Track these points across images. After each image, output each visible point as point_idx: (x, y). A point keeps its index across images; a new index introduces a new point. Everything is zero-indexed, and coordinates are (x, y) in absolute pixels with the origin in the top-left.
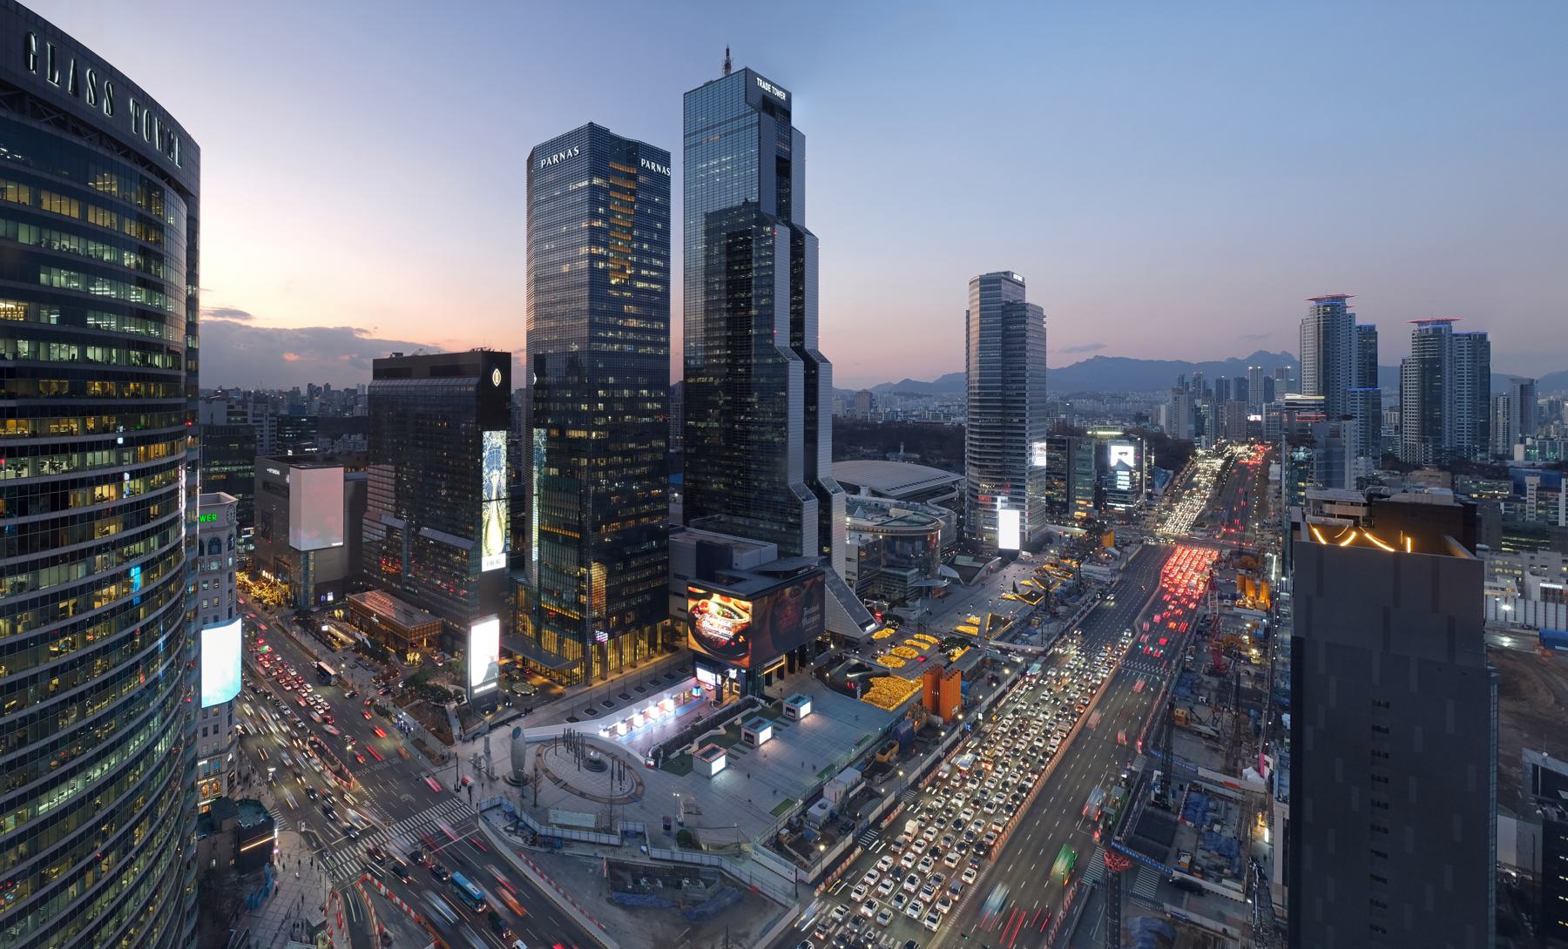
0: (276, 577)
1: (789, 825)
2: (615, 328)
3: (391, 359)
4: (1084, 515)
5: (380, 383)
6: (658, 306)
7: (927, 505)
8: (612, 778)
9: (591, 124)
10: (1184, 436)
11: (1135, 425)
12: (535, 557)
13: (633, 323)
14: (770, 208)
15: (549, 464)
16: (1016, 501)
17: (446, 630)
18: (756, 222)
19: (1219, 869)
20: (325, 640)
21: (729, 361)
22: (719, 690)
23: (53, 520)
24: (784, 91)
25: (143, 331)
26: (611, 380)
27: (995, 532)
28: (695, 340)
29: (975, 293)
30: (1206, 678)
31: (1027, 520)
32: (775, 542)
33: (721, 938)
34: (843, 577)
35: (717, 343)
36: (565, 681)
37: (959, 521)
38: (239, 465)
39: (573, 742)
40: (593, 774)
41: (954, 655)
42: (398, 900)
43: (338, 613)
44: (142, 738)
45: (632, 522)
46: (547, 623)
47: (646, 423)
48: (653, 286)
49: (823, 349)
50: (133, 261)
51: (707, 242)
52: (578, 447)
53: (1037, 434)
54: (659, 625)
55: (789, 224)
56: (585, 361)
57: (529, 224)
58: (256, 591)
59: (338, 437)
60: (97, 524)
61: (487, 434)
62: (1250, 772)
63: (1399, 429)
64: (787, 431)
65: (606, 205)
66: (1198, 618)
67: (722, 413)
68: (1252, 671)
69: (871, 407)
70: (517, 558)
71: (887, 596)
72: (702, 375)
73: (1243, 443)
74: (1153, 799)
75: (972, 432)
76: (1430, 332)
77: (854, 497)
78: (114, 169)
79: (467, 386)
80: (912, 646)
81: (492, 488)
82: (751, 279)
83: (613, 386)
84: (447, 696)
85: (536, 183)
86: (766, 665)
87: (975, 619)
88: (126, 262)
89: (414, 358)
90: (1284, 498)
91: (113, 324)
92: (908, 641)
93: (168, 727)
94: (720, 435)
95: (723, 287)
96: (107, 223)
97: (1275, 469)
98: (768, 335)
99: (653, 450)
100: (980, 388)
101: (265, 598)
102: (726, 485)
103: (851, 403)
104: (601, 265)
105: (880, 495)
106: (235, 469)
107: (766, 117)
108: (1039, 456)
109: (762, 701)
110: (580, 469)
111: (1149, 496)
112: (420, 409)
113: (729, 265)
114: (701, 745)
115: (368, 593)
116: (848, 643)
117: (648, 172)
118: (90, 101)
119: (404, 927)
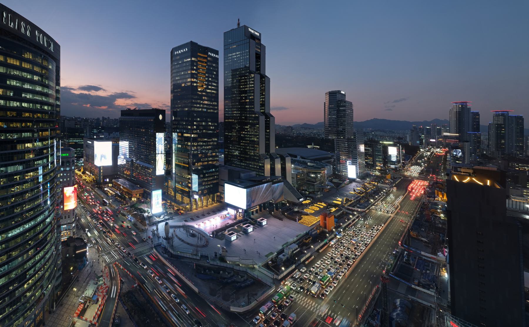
0: (91, 173)
1: (272, 260)
2: (200, 104)
3: (127, 110)
4: (380, 168)
6: (215, 98)
7: (322, 162)
8: (198, 239)
9: (191, 41)
11: (397, 141)
12: (174, 172)
13: (206, 102)
14: (253, 68)
15: (178, 144)
16: (353, 163)
17: (145, 192)
19: (429, 285)
20: (106, 193)
22: (236, 216)
23: (12, 153)
25: (41, 99)
26: (198, 119)
27: (347, 172)
29: (327, 97)
30: (424, 223)
31: (358, 169)
32: (256, 171)
33: (247, 295)
36: (184, 209)
37: (333, 168)
39: (187, 228)
41: (332, 210)
42: (126, 271)
43: (110, 185)
44: (42, 217)
45: (206, 163)
46: (178, 192)
47: (210, 133)
48: (213, 91)
50: (37, 78)
51: (232, 78)
52: (188, 139)
54: (216, 195)
58: (84, 177)
60: (26, 154)
61: (157, 134)
62: (440, 254)
65: (196, 66)
66: (421, 203)
70: (168, 172)
71: (308, 190)
73: (438, 148)
74: (405, 261)
76: (500, 115)
77: (295, 159)
78: (31, 52)
80: (317, 206)
83: (199, 121)
84: (145, 212)
85: (173, 59)
86: (251, 209)
88: (35, 79)
89: (135, 110)
91: (31, 96)
92: (315, 205)
93: (51, 214)
96: (28, 67)
97: (448, 156)
99: (212, 141)
101: (87, 179)
102: (239, 153)
103: (284, 130)
104: (195, 84)
105: (304, 159)
106: (77, 141)
107: (251, 40)
108: (362, 148)
109: (250, 220)
110: (188, 146)
111: (403, 163)
114: (229, 231)
115: (120, 179)
118: (23, 31)
119: (128, 279)
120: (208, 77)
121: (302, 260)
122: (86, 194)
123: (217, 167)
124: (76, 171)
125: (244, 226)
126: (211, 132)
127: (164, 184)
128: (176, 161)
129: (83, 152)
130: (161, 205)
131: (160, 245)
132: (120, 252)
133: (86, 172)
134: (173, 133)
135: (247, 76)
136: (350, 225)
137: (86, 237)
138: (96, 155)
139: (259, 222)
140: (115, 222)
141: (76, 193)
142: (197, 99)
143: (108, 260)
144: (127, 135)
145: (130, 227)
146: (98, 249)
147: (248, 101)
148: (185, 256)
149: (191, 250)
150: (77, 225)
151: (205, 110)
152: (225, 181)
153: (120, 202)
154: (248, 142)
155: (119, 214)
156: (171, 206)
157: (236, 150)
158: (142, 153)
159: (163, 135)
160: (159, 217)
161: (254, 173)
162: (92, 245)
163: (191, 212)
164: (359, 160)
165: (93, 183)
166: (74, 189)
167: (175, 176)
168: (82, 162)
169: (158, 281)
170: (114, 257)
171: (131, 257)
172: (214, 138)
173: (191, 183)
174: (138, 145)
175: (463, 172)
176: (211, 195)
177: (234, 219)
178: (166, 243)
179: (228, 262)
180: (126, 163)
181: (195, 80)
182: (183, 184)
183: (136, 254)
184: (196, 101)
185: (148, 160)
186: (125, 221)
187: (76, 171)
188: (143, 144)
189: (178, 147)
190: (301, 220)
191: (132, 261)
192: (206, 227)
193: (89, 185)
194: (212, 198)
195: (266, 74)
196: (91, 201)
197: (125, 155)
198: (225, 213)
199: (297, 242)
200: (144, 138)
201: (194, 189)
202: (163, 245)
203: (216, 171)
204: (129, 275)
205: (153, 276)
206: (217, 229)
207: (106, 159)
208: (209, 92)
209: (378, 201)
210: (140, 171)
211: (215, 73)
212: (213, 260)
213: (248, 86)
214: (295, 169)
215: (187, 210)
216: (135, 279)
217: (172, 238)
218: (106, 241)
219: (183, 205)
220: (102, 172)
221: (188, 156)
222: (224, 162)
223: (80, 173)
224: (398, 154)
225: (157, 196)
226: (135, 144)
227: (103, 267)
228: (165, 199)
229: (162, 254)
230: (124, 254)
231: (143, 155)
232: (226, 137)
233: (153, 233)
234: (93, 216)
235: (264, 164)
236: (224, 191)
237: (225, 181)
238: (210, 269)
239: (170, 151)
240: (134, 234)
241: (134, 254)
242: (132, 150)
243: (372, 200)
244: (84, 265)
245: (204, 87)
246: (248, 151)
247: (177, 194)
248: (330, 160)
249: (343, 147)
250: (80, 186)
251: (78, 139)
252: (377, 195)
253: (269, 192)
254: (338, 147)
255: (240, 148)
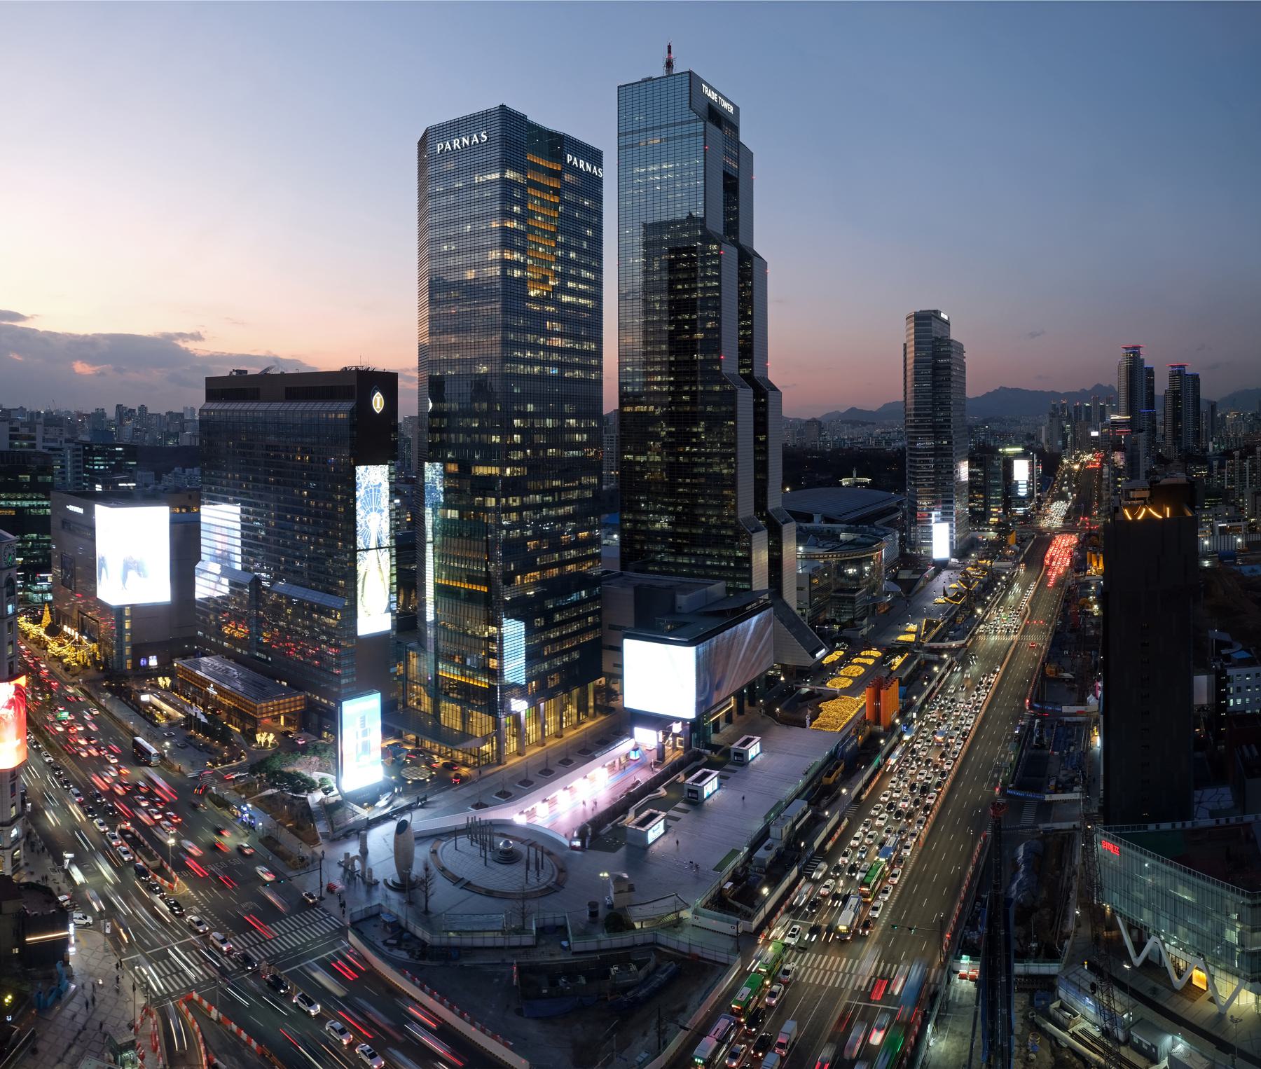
1: (735, 878)
2: (535, 347)
3: (230, 377)
4: (996, 520)
5: (215, 406)
7: (874, 526)
8: (528, 868)
10: (1056, 451)
12: (430, 617)
13: (558, 342)
15: (447, 505)
16: (945, 517)
17: (311, 706)
18: (701, 239)
20: (146, 714)
21: (672, 388)
24: (731, 103)
26: (530, 408)
27: (930, 544)
28: (632, 364)
29: (911, 329)
30: (1068, 635)
34: (794, 606)
35: (657, 368)
36: (471, 761)
37: (902, 539)
38: (32, 499)
39: (480, 833)
40: (504, 867)
42: (234, 1027)
43: (164, 682)
45: (555, 571)
46: (447, 694)
47: (574, 458)
48: (582, 301)
49: (773, 376)
51: (646, 256)
52: (486, 486)
53: (962, 453)
54: (591, 686)
55: (736, 243)
56: (496, 385)
57: (421, 220)
58: (54, 647)
59: (168, 470)
61: (360, 470)
63: (1163, 436)
64: (736, 462)
65: (522, 203)
67: (664, 445)
68: (1094, 621)
69: (820, 435)
70: (408, 620)
72: (641, 404)
73: (1089, 453)
75: (911, 455)
77: (808, 525)
79: (336, 412)
80: (859, 664)
81: (369, 535)
82: (695, 299)
84: (311, 786)
85: (430, 170)
86: (713, 712)
87: (913, 627)
89: (265, 377)
90: (1111, 490)
92: (855, 660)
94: (663, 470)
95: (665, 307)
97: (1106, 470)
98: (715, 360)
99: (582, 487)
100: (915, 415)
101: (66, 656)
102: (670, 524)
103: (800, 433)
104: (517, 273)
106: (26, 504)
108: (964, 471)
109: (708, 752)
110: (487, 510)
111: (1039, 498)
112: (272, 439)
113: (672, 283)
114: (637, 814)
115: (205, 659)
116: (800, 673)
117: (576, 171)
120: (566, 247)
121: (816, 844)
122: (65, 714)
123: (597, 581)
124: (23, 623)
125: (689, 781)
126: (576, 453)
127: (392, 670)
128: (437, 574)
129: (50, 548)
130: (379, 753)
131: (377, 916)
132: (209, 952)
133: (61, 629)
134: (427, 464)
135: (694, 250)
136: (934, 694)
137: (64, 886)
138: (103, 559)
139: (736, 754)
140: (186, 830)
141: (23, 710)
142: (526, 330)
143: (157, 984)
144: (234, 478)
145: (247, 852)
146: (115, 936)
147: (699, 336)
148: (478, 942)
149: (500, 915)
150: (27, 835)
151: (555, 371)
152: (624, 628)
153: (206, 748)
154: (703, 480)
155: (201, 797)
156: (421, 754)
157: (661, 513)
158: (298, 549)
159: (387, 473)
160: (372, 802)
161: (718, 588)
162: (89, 919)
163: (501, 767)
164: (958, 507)
165: (91, 673)
166: (16, 694)
167: (436, 636)
168: (45, 586)
169: (368, 1061)
170: (183, 971)
171: (256, 974)
172: (588, 475)
173: (499, 656)
174: (278, 517)
175: (1138, 499)
176: (575, 692)
177: (655, 763)
178: (400, 904)
179: (638, 926)
180: (231, 591)
181: (516, 256)
182: (469, 661)
183: (274, 960)
184: (520, 338)
185: (322, 577)
186: (228, 825)
187: (23, 623)
188: (301, 513)
189: (445, 520)
190: (817, 717)
191: (259, 990)
192: (558, 815)
193: (74, 680)
194: (578, 703)
195: (756, 248)
196: (83, 742)
197: (224, 558)
198: (625, 746)
199: (805, 794)
200: (307, 488)
201: (509, 678)
202: (390, 913)
203: (592, 599)
204: (247, 1044)
205: (350, 1044)
206: (596, 813)
207: (145, 576)
208: (569, 305)
209: (991, 607)
210: (288, 623)
211: (589, 233)
212: (584, 934)
213: (700, 285)
214: (806, 558)
215: (483, 763)
216: (274, 1059)
217: (424, 883)
218: (150, 906)
219: (469, 744)
220: (131, 630)
221: (487, 552)
222: (618, 562)
223: (37, 631)
224: (1030, 478)
225: (363, 719)
226: (269, 516)
227: (138, 1012)
228: (397, 727)
229: (386, 949)
230: (225, 961)
231: (301, 559)
232: (627, 471)
233: (346, 869)
234: (93, 802)
235: (749, 549)
236: (621, 666)
237: (624, 628)
238: (571, 971)
239: (412, 536)
240: (268, 878)
241: (267, 959)
242: (256, 538)
243: (979, 611)
244: (59, 995)
245: (551, 283)
246: (701, 512)
247: (443, 704)
248: (894, 516)
249: (923, 473)
250: (37, 681)
251: (29, 496)
252: (989, 594)
253: (765, 644)
254: (914, 473)
255: (675, 505)
